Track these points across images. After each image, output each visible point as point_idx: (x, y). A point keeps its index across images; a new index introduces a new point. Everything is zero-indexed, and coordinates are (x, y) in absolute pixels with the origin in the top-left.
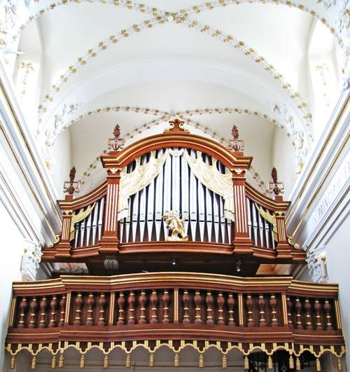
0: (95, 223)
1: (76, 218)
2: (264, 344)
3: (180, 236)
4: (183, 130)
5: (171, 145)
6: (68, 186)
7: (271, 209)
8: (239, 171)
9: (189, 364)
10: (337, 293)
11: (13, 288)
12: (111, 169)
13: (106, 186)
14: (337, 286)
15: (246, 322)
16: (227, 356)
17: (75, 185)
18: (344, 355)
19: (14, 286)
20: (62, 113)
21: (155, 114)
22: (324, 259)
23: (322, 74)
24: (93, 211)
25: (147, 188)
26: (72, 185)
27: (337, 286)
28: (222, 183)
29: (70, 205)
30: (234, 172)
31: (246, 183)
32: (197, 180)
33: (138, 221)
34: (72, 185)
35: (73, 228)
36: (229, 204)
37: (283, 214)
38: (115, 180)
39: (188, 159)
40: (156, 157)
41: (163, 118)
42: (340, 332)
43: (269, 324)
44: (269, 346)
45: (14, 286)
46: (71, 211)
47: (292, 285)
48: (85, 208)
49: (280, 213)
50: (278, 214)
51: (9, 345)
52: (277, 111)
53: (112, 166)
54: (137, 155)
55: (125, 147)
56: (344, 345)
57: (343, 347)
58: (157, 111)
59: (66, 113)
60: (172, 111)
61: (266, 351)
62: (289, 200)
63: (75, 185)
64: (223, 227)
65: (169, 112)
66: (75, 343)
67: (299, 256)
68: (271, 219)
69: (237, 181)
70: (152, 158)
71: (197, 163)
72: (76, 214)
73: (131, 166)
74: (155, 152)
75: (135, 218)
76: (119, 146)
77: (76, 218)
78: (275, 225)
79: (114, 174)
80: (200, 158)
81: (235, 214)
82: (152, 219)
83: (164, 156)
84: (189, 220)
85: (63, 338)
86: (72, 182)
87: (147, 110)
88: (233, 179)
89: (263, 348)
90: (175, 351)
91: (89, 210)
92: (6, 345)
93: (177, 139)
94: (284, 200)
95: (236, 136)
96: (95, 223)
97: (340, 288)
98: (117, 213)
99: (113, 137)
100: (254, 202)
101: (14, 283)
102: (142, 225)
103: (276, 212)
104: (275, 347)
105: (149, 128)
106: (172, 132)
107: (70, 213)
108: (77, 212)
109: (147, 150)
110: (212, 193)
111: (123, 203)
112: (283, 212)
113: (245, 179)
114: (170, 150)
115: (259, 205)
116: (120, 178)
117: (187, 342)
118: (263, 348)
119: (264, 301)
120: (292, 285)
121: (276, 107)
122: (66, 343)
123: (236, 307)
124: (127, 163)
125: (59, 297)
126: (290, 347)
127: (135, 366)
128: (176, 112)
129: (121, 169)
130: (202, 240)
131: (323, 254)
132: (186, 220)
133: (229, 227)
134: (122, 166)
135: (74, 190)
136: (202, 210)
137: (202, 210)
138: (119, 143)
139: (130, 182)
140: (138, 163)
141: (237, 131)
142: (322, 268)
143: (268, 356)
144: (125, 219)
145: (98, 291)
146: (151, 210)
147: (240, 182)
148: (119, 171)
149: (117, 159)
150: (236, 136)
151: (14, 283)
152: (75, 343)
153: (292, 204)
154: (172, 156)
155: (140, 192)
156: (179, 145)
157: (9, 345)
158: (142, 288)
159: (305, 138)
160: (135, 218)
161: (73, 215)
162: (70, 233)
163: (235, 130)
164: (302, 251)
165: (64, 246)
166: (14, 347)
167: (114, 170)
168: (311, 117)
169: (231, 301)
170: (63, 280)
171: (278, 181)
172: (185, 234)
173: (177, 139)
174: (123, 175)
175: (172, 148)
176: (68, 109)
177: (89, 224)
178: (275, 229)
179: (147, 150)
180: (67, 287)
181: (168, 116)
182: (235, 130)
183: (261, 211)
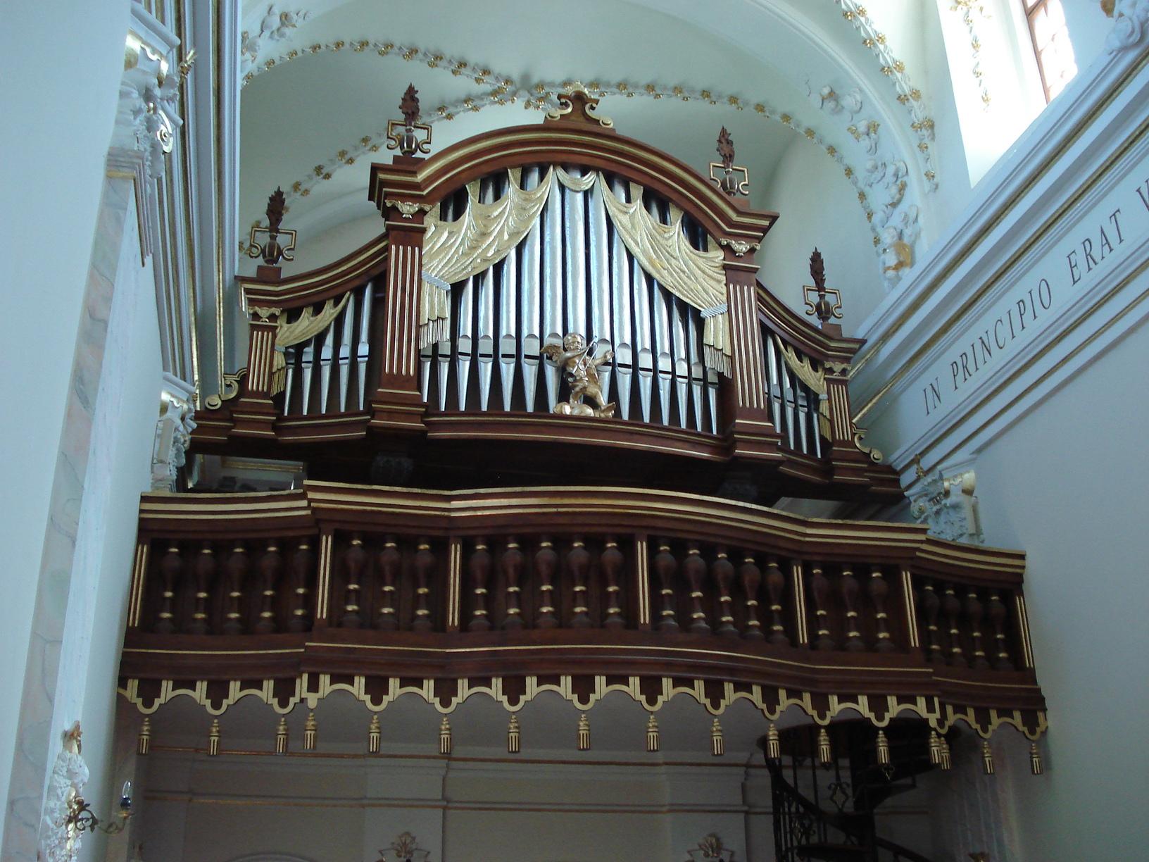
0: (345, 351)
1: (290, 333)
2: (865, 698)
3: (591, 401)
4: (597, 122)
5: (564, 158)
6: (263, 239)
7: (814, 355)
8: (742, 247)
9: (541, 753)
10: (1020, 576)
11: (141, 511)
12: (400, 205)
13: (387, 249)
14: (1022, 557)
15: (812, 635)
16: (829, 728)
17: (282, 240)
18: (1044, 733)
19: (148, 506)
20: (258, 31)
21: (478, 80)
22: (968, 492)
23: (968, 21)
24: (339, 321)
25: (498, 268)
26: (273, 238)
27: (1022, 557)
28: (699, 275)
29: (278, 292)
30: (728, 249)
31: (759, 285)
32: (631, 257)
33: (474, 356)
34: (273, 238)
35: (279, 360)
36: (717, 333)
37: (844, 372)
38: (412, 236)
39: (609, 199)
40: (522, 187)
41: (495, 93)
42: (1030, 676)
43: (870, 643)
44: (878, 705)
45: (148, 506)
46: (277, 311)
47: (924, 547)
48: (318, 309)
49: (838, 367)
50: (831, 371)
51: (133, 685)
52: (830, 105)
53: (404, 198)
54: (471, 175)
55: (435, 148)
56: (1045, 710)
57: (1040, 715)
58: (486, 72)
59: (267, 33)
60: (526, 78)
61: (872, 716)
62: (860, 337)
63: (282, 240)
64: (697, 391)
65: (516, 76)
66: (259, 686)
67: (882, 482)
68: (815, 379)
69: (735, 272)
70: (512, 189)
71: (637, 220)
72: (289, 322)
73: (454, 203)
74: (518, 173)
75: (465, 346)
76: (418, 146)
77: (290, 333)
78: (823, 396)
79: (407, 220)
80: (638, 204)
81: (732, 358)
82: (491, 352)
83: (547, 188)
84: (613, 364)
85: (315, 666)
86: (274, 228)
87: (463, 64)
88: (725, 267)
89: (863, 706)
90: (579, 706)
91: (329, 312)
92: (122, 682)
93: (574, 143)
94: (845, 334)
95: (728, 158)
96: (345, 351)
97: (1029, 562)
98: (419, 327)
99: (400, 117)
100: (773, 334)
101: (144, 499)
102: (508, 370)
103: (828, 365)
104: (894, 708)
105: (449, 117)
106: (565, 124)
107: (273, 317)
108: (293, 315)
109: (495, 167)
110: (668, 295)
111: (434, 302)
112: (844, 366)
113: (755, 271)
114: (561, 172)
115: (785, 343)
116: (423, 231)
117: (677, 682)
118: (863, 706)
119: (855, 584)
120: (924, 547)
121: (832, 95)
122: (325, 680)
123: (787, 598)
124: (443, 193)
125: (287, 546)
126: (930, 709)
127: (450, 759)
128: (535, 80)
129: (427, 208)
130: (666, 422)
131: (969, 477)
132: (606, 364)
133: (712, 394)
134: (432, 202)
135: (280, 253)
136: (644, 340)
137: (644, 340)
138: (420, 135)
139: (447, 249)
140: (472, 200)
141: (730, 143)
142: (967, 512)
143: (820, 727)
144: (435, 346)
145: (414, 531)
146: (508, 326)
147: (743, 275)
148: (422, 213)
149: (420, 177)
150: (728, 158)
151: (144, 499)
152: (259, 686)
153: (866, 346)
154: (562, 188)
155: (479, 279)
156: (585, 161)
157: (133, 685)
158: (610, 530)
159: (913, 180)
160: (465, 346)
161: (281, 322)
162: (271, 374)
163: (724, 138)
164: (890, 469)
165: (259, 410)
166: (149, 691)
167: (408, 209)
168: (932, 126)
169: (775, 577)
170: (311, 495)
171: (826, 285)
172: (603, 399)
173: (574, 143)
174: (431, 222)
175: (566, 167)
176: (275, 22)
177: (327, 353)
178: (824, 408)
179: (495, 167)
180: (320, 519)
181: (509, 88)
182: (724, 138)
183: (790, 356)
